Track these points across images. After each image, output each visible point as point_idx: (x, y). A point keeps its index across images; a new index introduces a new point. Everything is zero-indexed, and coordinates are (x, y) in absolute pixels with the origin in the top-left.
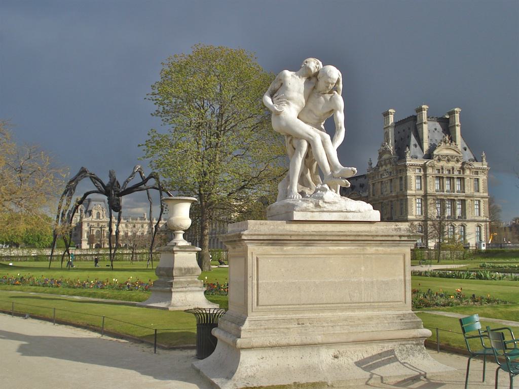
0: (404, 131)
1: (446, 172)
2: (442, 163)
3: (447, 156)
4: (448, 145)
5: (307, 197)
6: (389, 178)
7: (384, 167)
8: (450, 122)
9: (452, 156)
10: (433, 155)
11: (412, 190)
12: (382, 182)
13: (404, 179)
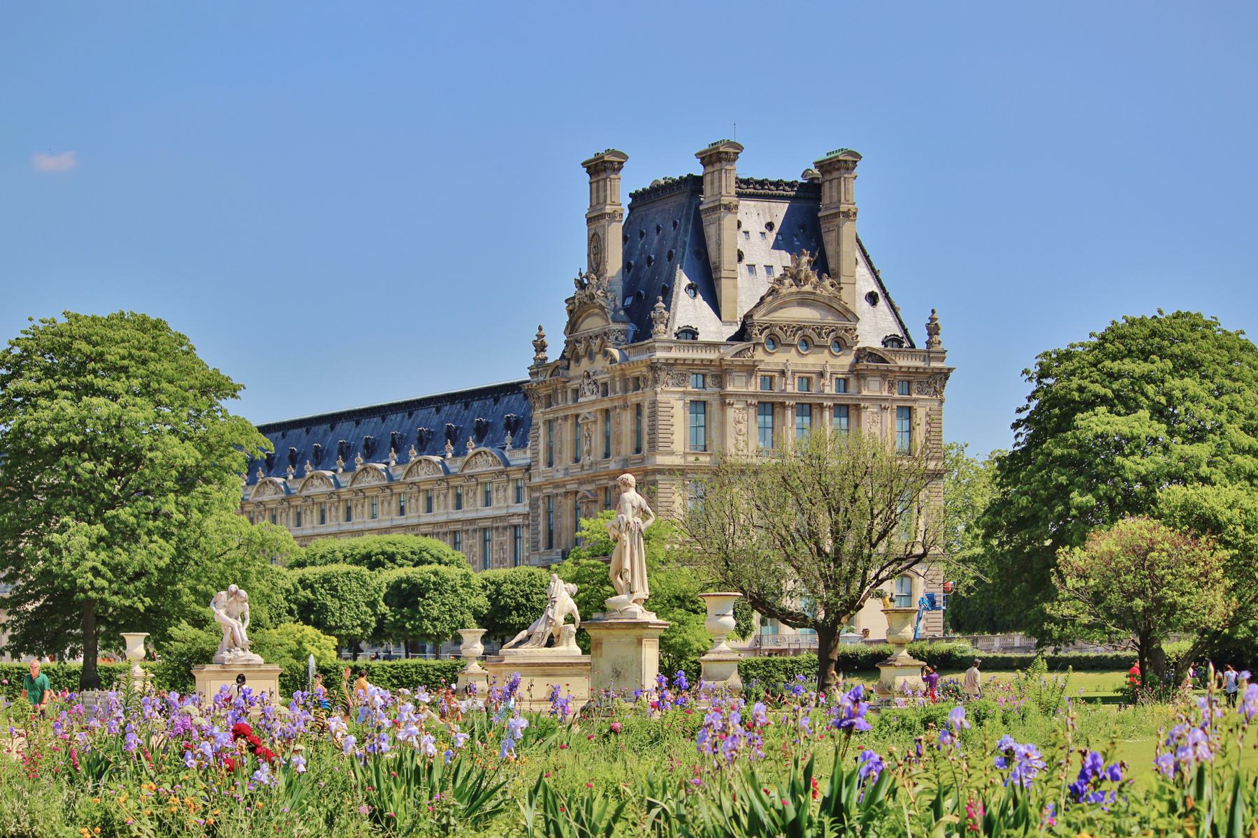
1: (792, 387)
2: (780, 359)
3: (800, 328)
4: (808, 288)
5: (1067, 630)
6: (599, 406)
7: (585, 362)
8: (826, 200)
9: (818, 330)
10: (752, 325)
11: (672, 453)
12: (577, 416)
13: (646, 412)
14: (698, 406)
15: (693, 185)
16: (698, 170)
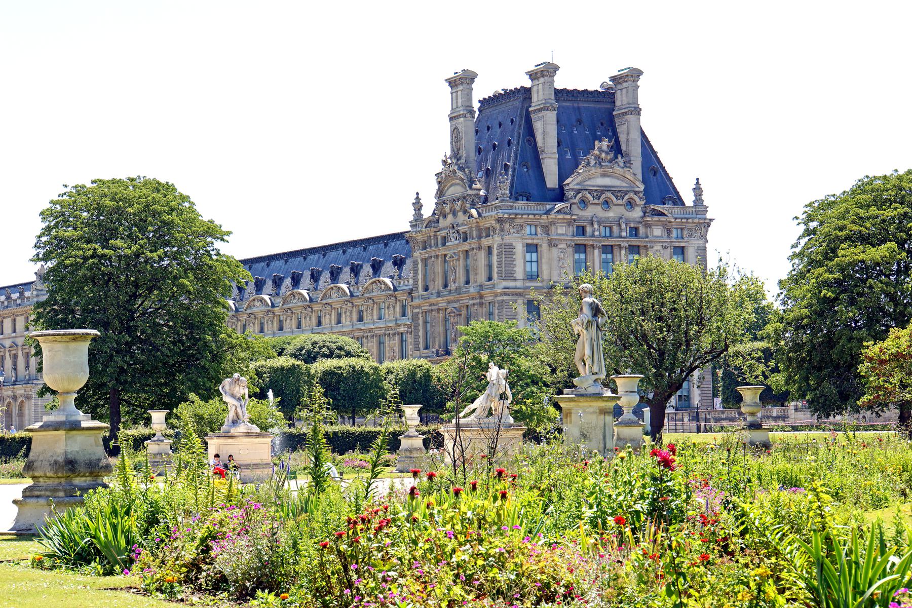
0: (500, 125)
14: (532, 248)
15: (525, 93)
16: (528, 83)
